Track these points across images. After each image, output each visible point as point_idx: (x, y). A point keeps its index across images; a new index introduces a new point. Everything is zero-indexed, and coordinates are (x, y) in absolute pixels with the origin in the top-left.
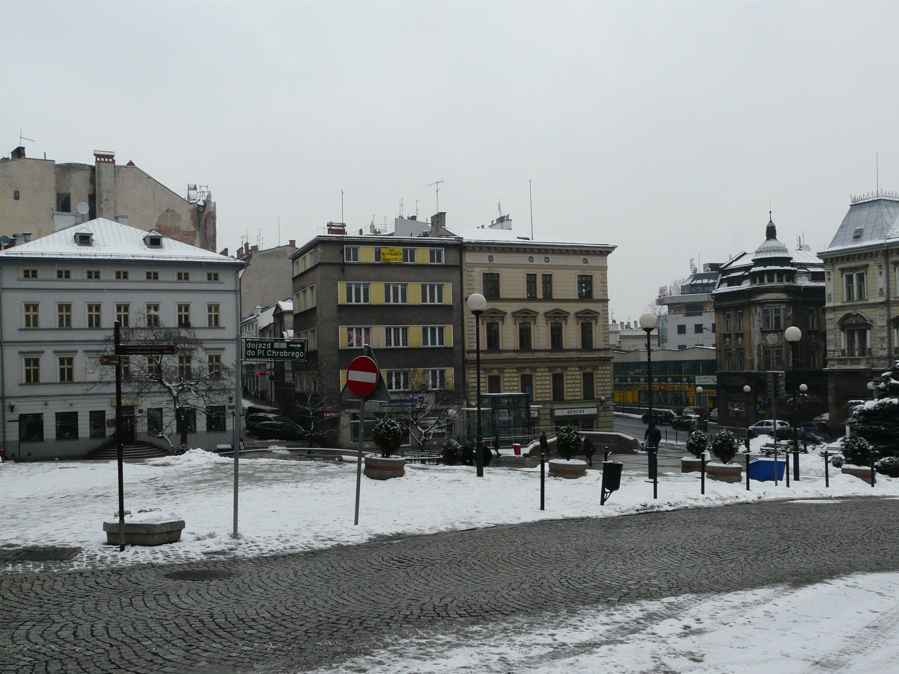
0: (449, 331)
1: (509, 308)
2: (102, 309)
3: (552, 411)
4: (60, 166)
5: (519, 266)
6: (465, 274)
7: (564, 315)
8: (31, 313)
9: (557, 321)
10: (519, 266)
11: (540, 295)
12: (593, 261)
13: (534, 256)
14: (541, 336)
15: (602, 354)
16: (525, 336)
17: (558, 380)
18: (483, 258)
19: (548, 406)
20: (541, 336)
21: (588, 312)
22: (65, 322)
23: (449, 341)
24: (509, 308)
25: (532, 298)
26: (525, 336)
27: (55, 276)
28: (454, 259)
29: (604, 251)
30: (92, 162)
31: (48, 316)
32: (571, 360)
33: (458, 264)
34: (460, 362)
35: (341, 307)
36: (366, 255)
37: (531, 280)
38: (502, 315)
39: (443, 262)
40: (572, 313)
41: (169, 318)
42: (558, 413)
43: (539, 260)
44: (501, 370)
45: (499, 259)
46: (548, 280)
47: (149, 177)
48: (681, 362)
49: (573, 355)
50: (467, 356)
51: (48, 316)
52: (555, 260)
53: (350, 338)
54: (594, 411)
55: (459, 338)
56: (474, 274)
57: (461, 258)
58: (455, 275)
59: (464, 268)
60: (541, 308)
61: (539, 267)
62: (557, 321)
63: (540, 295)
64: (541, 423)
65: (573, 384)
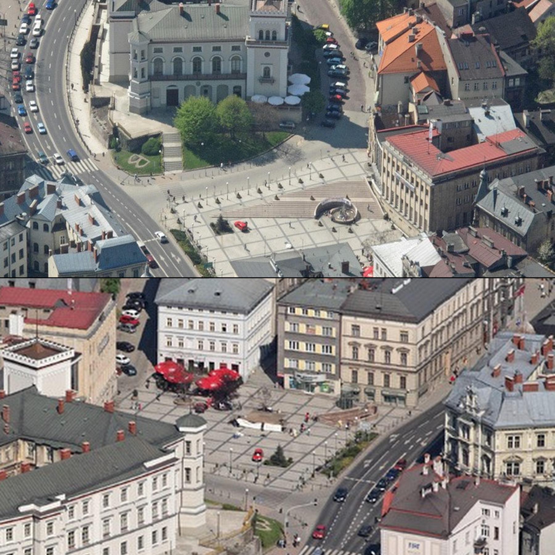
16: (371, 355)
20: (379, 356)
21: (355, 343)
22: (201, 328)
25: (376, 339)
26: (371, 355)
37: (376, 331)
42: (384, 393)
60: (380, 344)
62: (388, 351)
63: (380, 338)
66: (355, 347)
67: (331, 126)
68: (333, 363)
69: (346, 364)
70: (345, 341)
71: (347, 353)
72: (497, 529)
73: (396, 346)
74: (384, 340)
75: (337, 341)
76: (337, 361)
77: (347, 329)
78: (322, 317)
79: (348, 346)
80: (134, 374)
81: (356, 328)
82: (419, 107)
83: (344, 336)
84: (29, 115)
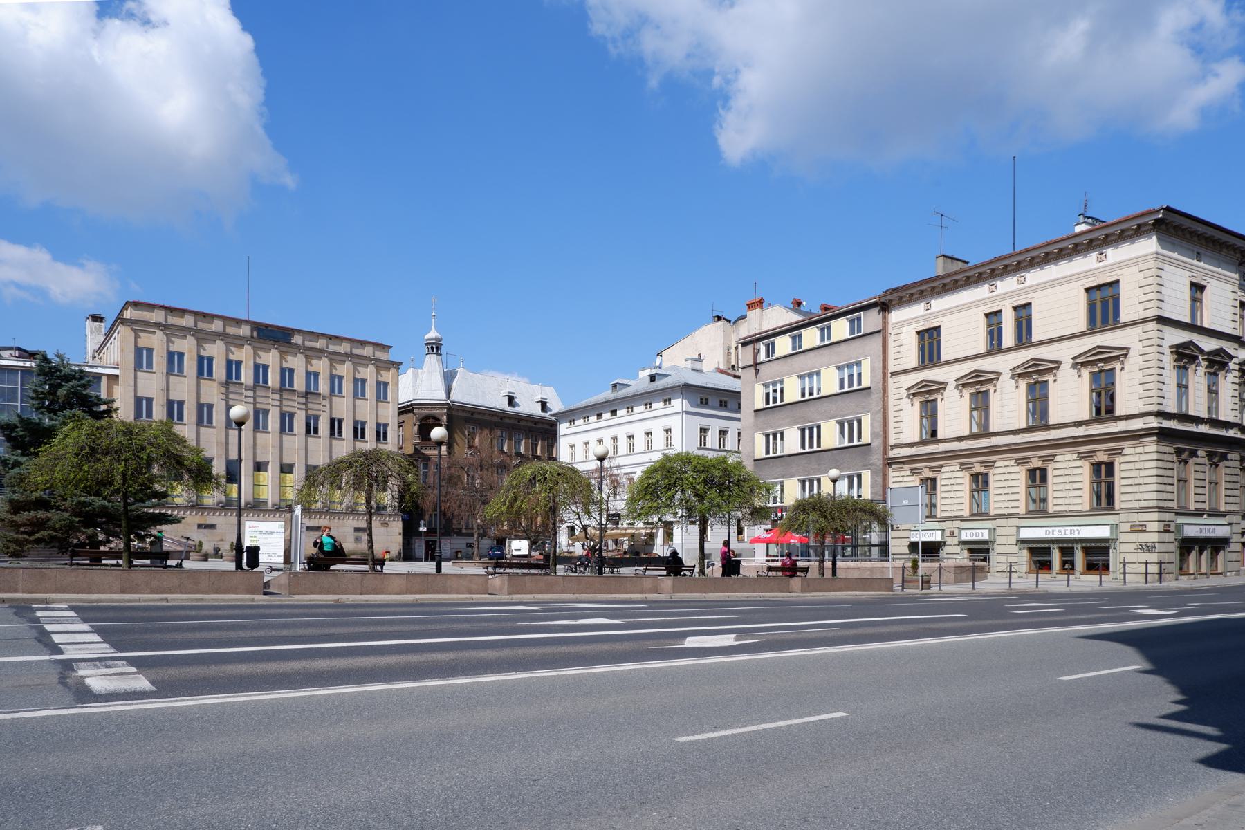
1: (1065, 353)
24: (1065, 353)
28: (871, 320)
33: (880, 328)
34: (880, 463)
44: (938, 469)
46: (1023, 313)
49: (1138, 424)
55: (879, 429)
56: (902, 336)
57: (884, 318)
59: (890, 330)
60: (1003, 364)
61: (1005, 296)
64: (998, 549)
68: (865, 467)
69: (902, 461)
75: (876, 396)
76: (877, 459)
77: (906, 350)
81: (930, 339)
83: (894, 374)
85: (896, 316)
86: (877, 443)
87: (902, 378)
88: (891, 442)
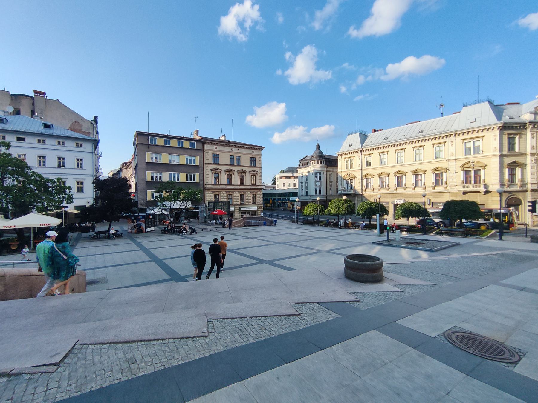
0: (198, 176)
1: (223, 168)
2: (46, 158)
3: (240, 208)
4: (12, 95)
5: (228, 152)
6: (205, 153)
7: (245, 172)
8: (80, 162)
9: (242, 173)
10: (228, 152)
11: (236, 164)
12: (256, 152)
13: (240, 149)
14: (236, 180)
15: (259, 187)
16: (230, 179)
17: (242, 197)
18: (212, 147)
19: (238, 206)
20: (236, 180)
21: (217, 169)
23: (198, 180)
24: (223, 168)
25: (232, 165)
26: (230, 179)
27: (57, 144)
28: (200, 146)
29: (260, 148)
30: (33, 95)
31: (71, 162)
32: (247, 189)
35: (147, 163)
36: (161, 142)
37: (232, 158)
38: (220, 171)
39: (195, 148)
40: (223, 170)
41: (530, 204)
42: (242, 209)
43: (235, 150)
44: (245, 192)
45: (219, 148)
46: (239, 159)
47: (65, 106)
48: (285, 193)
49: (248, 187)
50: (205, 186)
51: (71, 162)
52: (242, 150)
53: (174, 177)
54: (256, 209)
58: (200, 153)
60: (236, 169)
62: (242, 173)
63: (236, 164)
65: (248, 198)
66: (216, 173)
67: (370, 163)
69: (209, 189)
70: (208, 169)
71: (210, 179)
72: (281, 172)
73: (248, 170)
74: (239, 165)
75: (201, 169)
77: (209, 159)
78: (184, 146)
79: (210, 173)
80: (25, 155)
81: (216, 157)
82: (203, 214)
84: (529, 168)
85: (207, 147)
86: (202, 183)
87: (209, 166)
88: (205, 183)
